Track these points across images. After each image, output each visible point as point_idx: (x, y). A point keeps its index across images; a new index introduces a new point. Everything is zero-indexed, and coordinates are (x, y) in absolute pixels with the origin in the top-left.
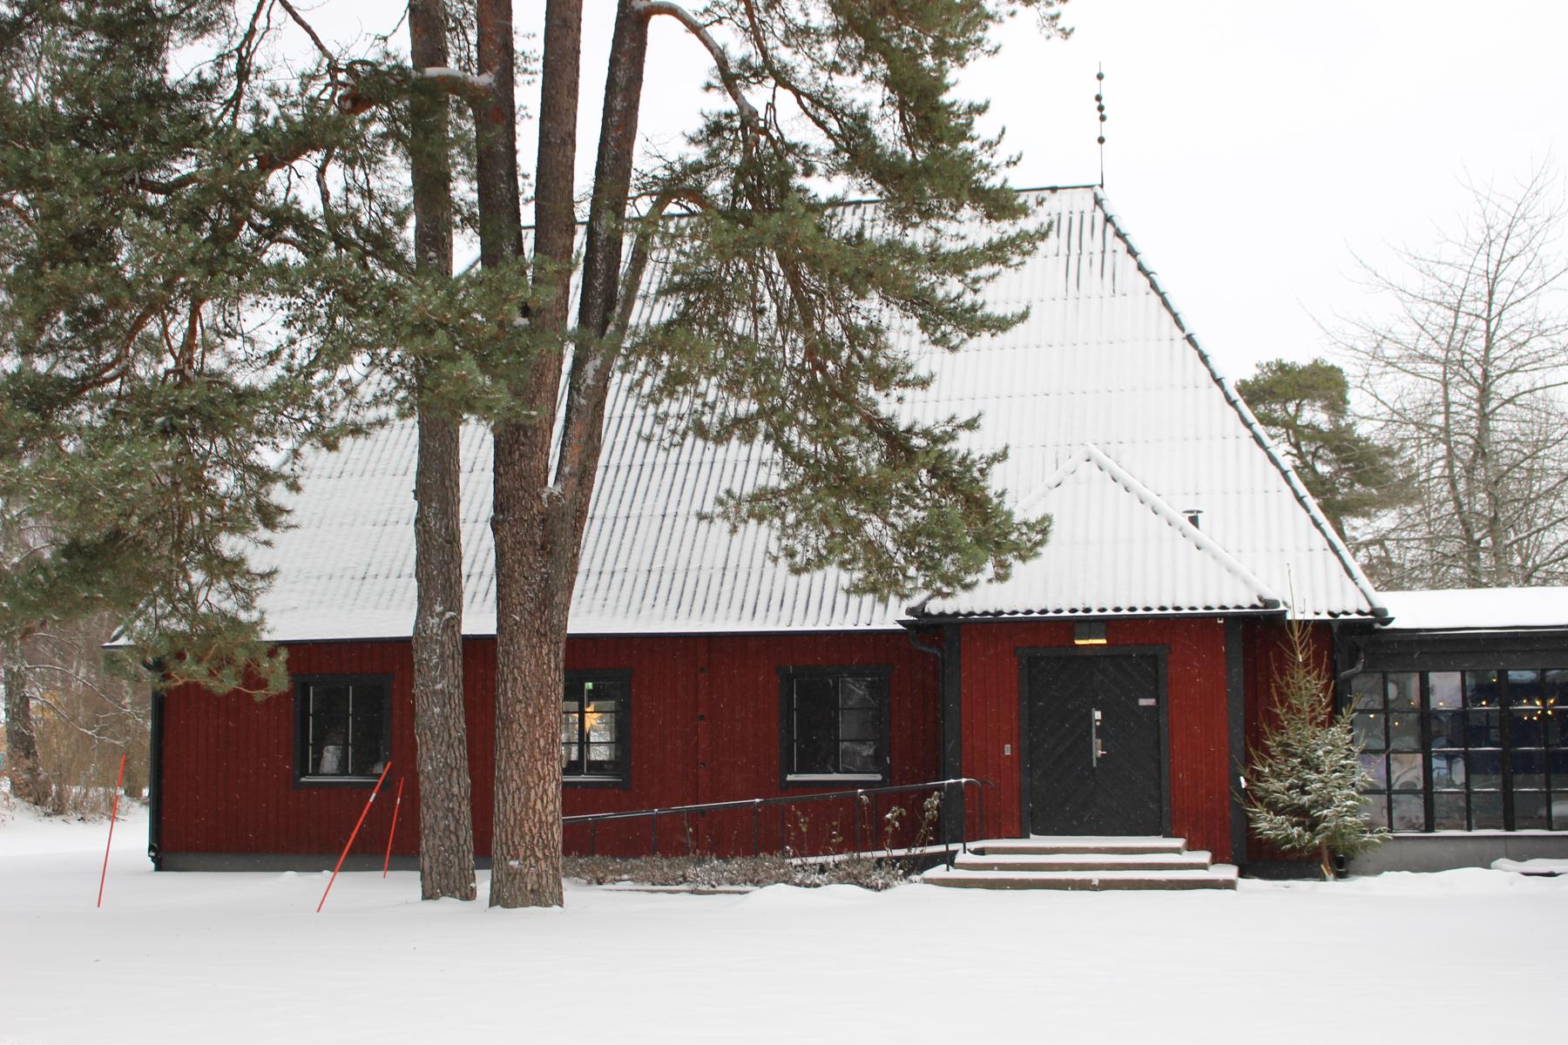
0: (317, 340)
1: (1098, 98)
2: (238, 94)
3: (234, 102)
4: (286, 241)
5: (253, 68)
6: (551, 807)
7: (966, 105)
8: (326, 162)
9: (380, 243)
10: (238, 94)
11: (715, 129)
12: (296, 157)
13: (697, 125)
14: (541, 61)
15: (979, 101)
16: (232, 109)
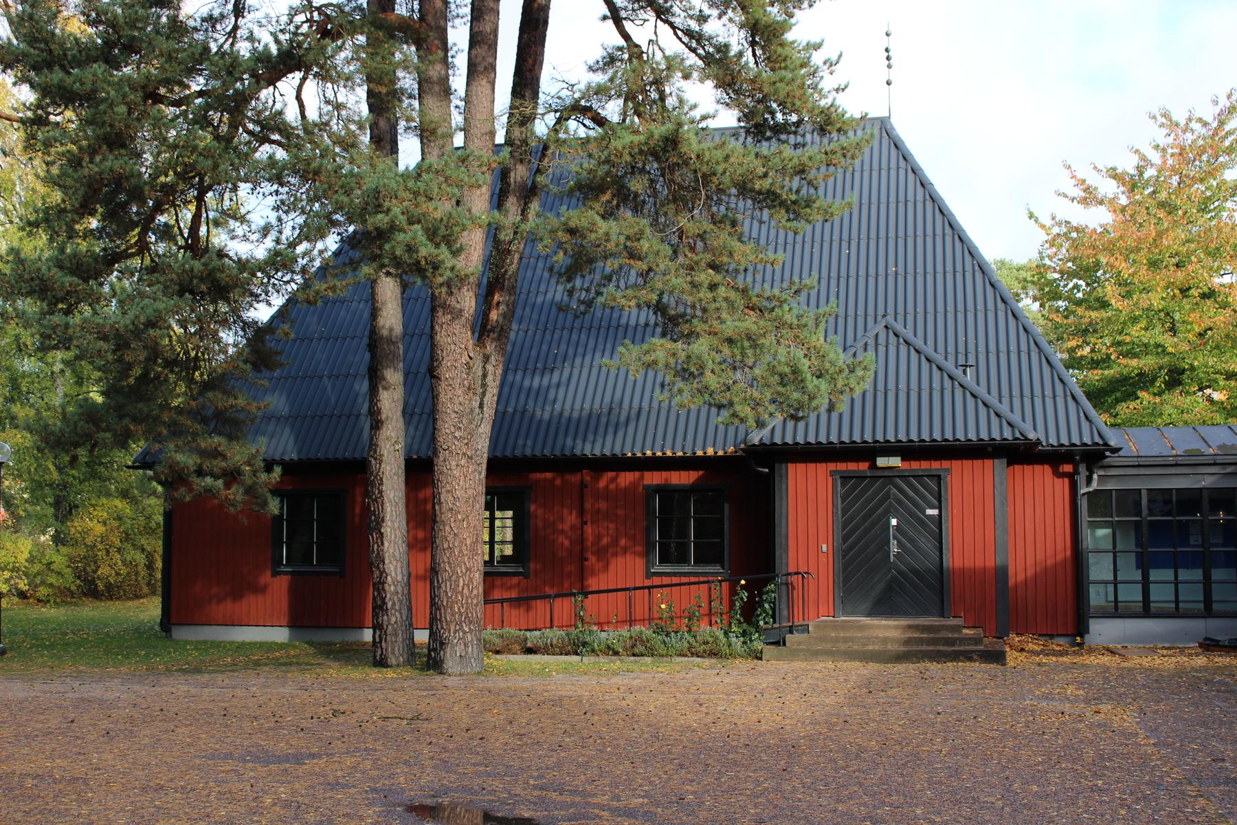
0: (300, 220)
1: (887, 50)
2: (236, 28)
3: (233, 33)
4: (274, 142)
5: (246, 6)
6: (475, 592)
7: (804, 43)
8: (304, 80)
9: (348, 144)
10: (236, 28)
11: (611, 60)
12: (279, 79)
13: (597, 54)
14: (470, 6)
15: (815, 39)
16: (231, 40)
